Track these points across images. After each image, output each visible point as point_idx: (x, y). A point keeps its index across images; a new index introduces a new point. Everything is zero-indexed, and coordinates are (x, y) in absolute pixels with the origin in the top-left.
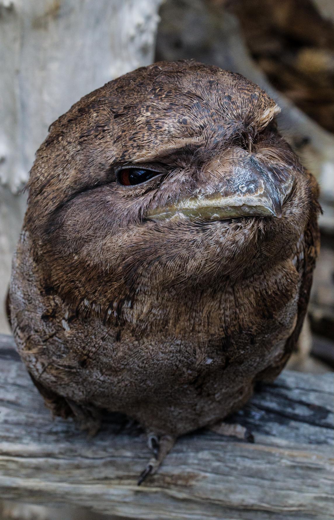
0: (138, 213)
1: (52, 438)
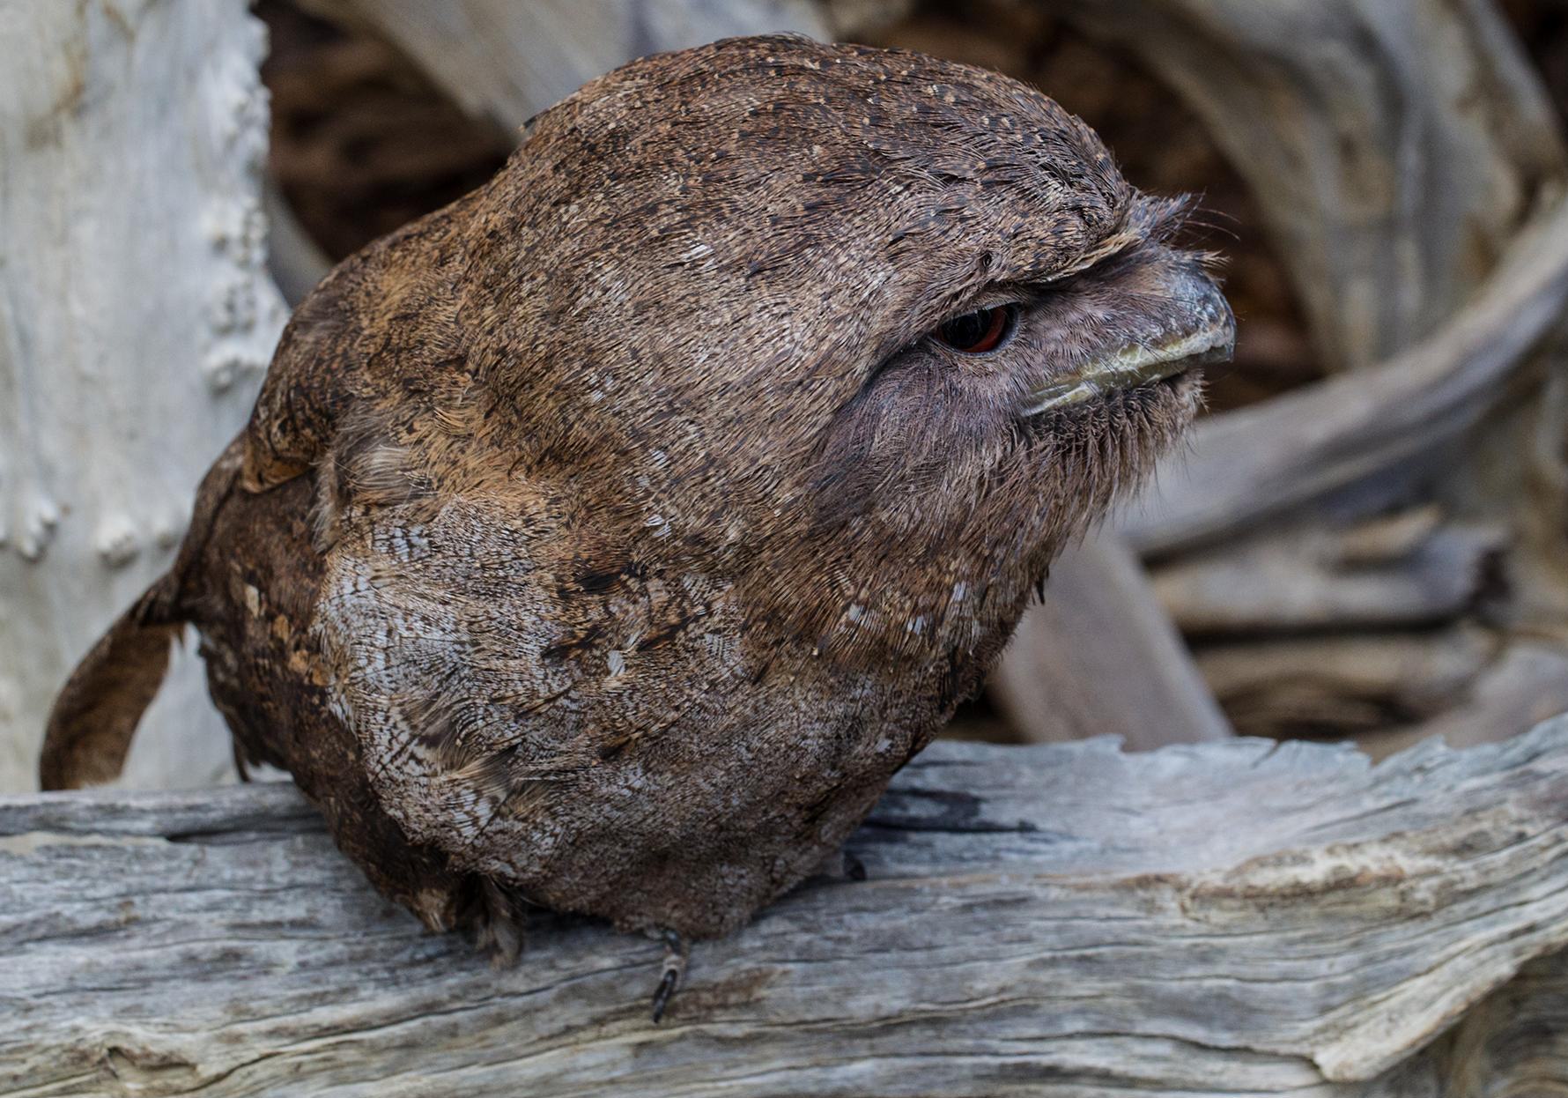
1: (421, 971)
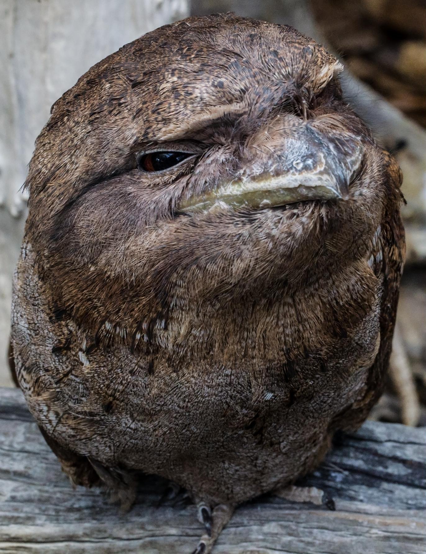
0: (167, 205)
1: (73, 516)
